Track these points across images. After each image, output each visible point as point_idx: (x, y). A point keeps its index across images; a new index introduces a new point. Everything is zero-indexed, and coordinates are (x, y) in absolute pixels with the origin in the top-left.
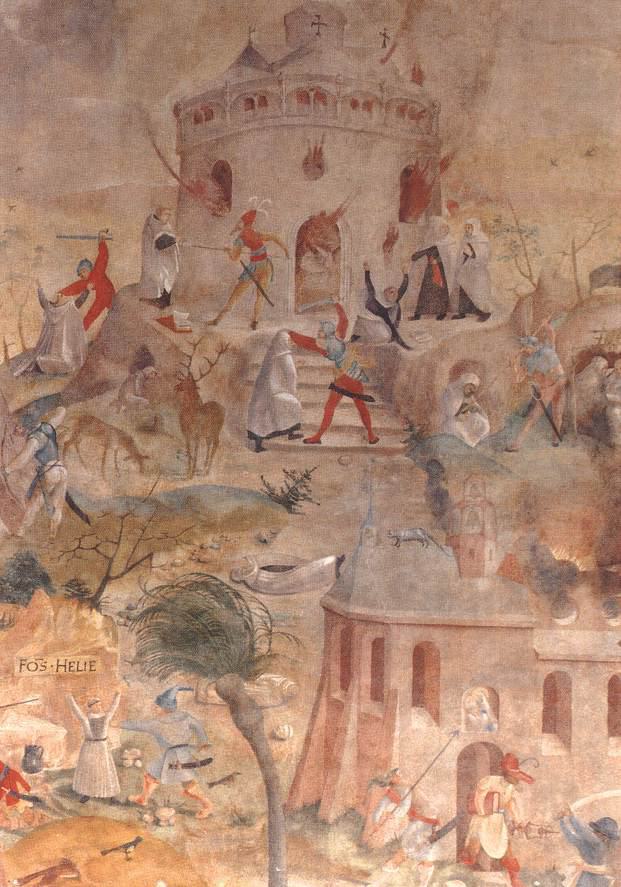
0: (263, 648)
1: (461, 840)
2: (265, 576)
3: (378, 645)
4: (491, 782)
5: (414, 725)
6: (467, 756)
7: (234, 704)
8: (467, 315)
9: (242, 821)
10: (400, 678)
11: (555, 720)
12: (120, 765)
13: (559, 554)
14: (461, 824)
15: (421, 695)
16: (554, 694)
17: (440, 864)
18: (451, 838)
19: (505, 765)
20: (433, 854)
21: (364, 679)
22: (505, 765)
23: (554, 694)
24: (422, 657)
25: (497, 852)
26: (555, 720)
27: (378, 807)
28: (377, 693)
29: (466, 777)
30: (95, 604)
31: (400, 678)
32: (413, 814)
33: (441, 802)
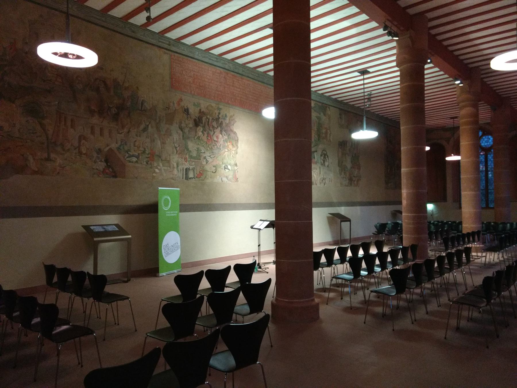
0: (46, 115)
1: (79, 150)
2: (46, 103)
3: (65, 118)
4: (83, 141)
5: (71, 131)
6: (80, 137)
7: (41, 125)
8: (132, 279)
9: (43, 143)
10: (69, 123)
11: (93, 133)
12: (19, 131)
13: (93, 108)
14: (79, 147)
15: (72, 126)
16: (92, 128)
17: (76, 153)
18: (77, 149)
19: (85, 138)
20: (75, 152)
21: (63, 123)
22: (85, 138)
23: (92, 128)
24: (72, 121)
25: (84, 152)
26: (93, 133)
27: (488, 266)
28: (65, 124)
29: (80, 141)
30: (13, 102)
31: (69, 123)
32: (72, 145)
33: (76, 144)
